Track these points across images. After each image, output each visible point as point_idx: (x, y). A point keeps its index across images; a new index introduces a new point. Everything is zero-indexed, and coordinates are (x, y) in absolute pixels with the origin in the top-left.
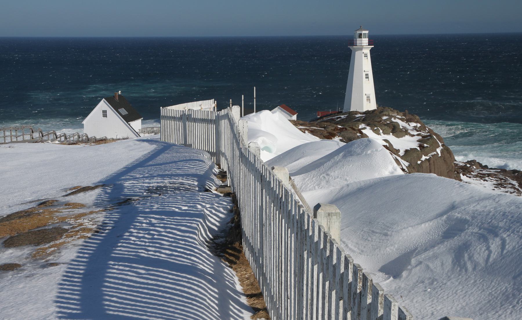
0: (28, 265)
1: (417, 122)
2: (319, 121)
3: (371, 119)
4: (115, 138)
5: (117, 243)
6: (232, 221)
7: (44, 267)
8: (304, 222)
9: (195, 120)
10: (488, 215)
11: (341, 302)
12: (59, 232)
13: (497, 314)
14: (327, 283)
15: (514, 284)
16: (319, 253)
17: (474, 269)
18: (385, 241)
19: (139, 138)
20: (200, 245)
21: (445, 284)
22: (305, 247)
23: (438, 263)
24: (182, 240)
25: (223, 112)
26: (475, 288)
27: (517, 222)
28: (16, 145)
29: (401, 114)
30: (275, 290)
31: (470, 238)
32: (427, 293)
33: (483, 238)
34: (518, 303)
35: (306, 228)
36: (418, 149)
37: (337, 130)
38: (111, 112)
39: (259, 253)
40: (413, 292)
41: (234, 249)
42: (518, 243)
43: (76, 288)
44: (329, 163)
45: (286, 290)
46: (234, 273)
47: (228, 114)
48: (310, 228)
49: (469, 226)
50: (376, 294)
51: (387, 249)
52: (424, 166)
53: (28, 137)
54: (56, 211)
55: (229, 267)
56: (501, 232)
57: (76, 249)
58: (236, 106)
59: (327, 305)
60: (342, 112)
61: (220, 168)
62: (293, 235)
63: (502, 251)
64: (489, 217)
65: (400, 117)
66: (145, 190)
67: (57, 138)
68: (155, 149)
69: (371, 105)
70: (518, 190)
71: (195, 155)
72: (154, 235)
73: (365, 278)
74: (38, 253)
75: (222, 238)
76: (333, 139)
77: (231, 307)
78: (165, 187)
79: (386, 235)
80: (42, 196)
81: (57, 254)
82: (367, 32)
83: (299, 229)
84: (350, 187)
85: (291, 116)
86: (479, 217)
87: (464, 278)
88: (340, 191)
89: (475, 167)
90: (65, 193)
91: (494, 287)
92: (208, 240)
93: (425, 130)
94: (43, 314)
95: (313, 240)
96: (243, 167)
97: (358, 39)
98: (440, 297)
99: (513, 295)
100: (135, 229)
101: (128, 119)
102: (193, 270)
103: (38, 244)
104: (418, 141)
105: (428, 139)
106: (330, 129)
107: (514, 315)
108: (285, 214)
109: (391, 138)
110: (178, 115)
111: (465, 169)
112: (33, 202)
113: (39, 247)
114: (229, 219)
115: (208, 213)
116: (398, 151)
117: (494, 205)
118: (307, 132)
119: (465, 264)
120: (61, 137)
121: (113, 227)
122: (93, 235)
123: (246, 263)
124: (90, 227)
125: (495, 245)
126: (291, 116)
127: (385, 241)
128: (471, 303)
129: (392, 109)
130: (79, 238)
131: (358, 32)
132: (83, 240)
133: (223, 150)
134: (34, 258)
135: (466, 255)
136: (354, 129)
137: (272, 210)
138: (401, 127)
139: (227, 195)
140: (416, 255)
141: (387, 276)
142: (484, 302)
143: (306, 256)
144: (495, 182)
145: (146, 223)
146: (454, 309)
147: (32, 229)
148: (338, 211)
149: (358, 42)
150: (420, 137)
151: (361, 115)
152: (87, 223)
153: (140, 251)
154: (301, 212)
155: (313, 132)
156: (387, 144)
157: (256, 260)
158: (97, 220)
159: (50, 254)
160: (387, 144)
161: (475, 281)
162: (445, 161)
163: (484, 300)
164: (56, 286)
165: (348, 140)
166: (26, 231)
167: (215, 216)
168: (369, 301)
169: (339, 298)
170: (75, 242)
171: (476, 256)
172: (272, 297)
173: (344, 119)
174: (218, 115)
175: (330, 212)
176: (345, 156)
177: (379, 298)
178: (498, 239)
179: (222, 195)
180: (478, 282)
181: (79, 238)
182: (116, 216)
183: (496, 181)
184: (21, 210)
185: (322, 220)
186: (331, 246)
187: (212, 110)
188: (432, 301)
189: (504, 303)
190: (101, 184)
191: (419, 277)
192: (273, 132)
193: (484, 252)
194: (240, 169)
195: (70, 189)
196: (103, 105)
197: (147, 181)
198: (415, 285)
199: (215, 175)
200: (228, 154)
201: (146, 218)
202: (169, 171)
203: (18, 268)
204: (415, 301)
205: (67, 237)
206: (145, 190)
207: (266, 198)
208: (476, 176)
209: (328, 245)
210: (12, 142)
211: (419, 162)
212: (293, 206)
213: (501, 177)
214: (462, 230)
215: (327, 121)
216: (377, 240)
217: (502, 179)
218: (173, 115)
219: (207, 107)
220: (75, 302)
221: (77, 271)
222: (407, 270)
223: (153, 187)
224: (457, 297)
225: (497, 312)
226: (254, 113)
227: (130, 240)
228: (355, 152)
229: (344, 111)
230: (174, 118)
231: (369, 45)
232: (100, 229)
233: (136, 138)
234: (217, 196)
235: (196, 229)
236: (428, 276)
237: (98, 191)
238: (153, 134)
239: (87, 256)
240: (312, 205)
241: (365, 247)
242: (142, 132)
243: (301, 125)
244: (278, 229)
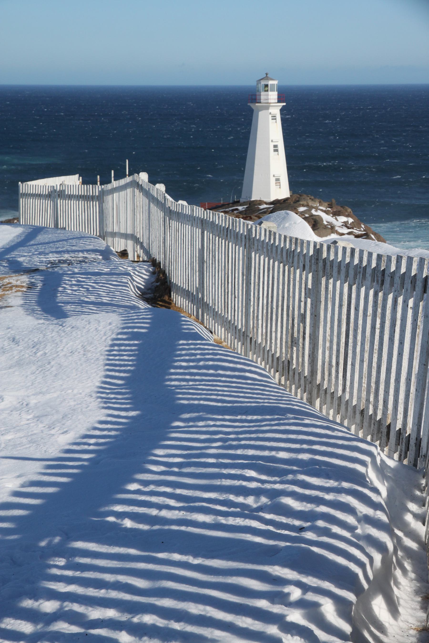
1: (348, 216)
6: (157, 280)
9: (70, 197)
22: (252, 250)
29: (326, 204)
60: (238, 202)
65: (324, 209)
69: (283, 192)
82: (275, 82)
92: (138, 295)
93: (360, 227)
114: (153, 280)
129: (312, 197)
131: (263, 83)
138: (325, 223)
145: (75, 281)
148: (275, 225)
149: (262, 97)
151: (268, 206)
167: (141, 277)
202: (62, 248)
229: (242, 200)
230: (39, 196)
231: (279, 101)
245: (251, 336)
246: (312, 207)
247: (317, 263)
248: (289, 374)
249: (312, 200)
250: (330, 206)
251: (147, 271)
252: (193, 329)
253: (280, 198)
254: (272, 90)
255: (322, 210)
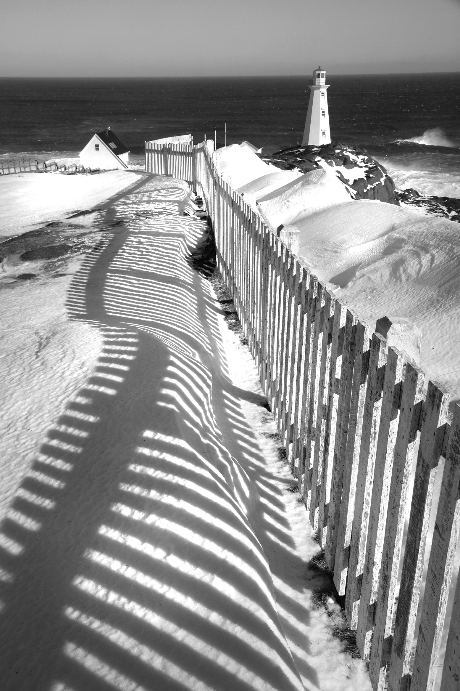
0: (42, 275)
1: (365, 155)
2: (281, 154)
3: (326, 152)
4: (107, 169)
5: (113, 258)
6: (208, 240)
7: (54, 277)
8: (269, 240)
9: (175, 153)
10: (422, 235)
11: (299, 306)
12: (65, 249)
13: (423, 316)
14: (288, 291)
15: (439, 292)
16: (281, 266)
17: (407, 280)
18: (335, 257)
19: (127, 169)
20: (181, 260)
21: (383, 292)
22: (269, 262)
23: (378, 275)
24: (166, 256)
25: (199, 146)
26: (407, 295)
27: (446, 241)
28: (24, 175)
30: (243, 297)
31: (405, 255)
32: (367, 299)
33: (416, 254)
34: (440, 307)
35: (271, 245)
36: (365, 179)
37: (297, 162)
38: (103, 146)
39: (230, 267)
40: (356, 299)
41: (209, 264)
42: (445, 258)
43: (81, 294)
44: (290, 191)
45: (253, 297)
46: (210, 283)
47: (203, 147)
48: (275, 245)
49: (405, 244)
50: (328, 300)
51: (337, 264)
52: (369, 194)
53: (34, 168)
54: (62, 231)
55: (206, 278)
56: (431, 249)
57: (80, 262)
58: (210, 140)
59: (287, 308)
61: (196, 195)
62: (260, 251)
63: (431, 265)
64: (423, 236)
65: (351, 151)
66: (134, 214)
67: (58, 169)
68: (142, 179)
69: (326, 140)
70: (446, 214)
71: (175, 184)
72: (142, 252)
73: (320, 286)
74: (49, 265)
75: (199, 254)
76: (293, 170)
77: (207, 311)
78: (150, 211)
79: (336, 252)
80: (49, 219)
81: (64, 267)
82: (324, 72)
83: (265, 247)
84: (307, 212)
85: (257, 150)
86: (414, 237)
87: (399, 288)
88: (297, 217)
89: (412, 195)
90: (67, 216)
91: (422, 294)
92: (188, 256)
93: (372, 162)
94: (57, 314)
95: (277, 255)
96: (216, 193)
97: (317, 79)
98: (378, 303)
99: (438, 300)
100: (127, 246)
101: (117, 152)
102: (175, 281)
103: (49, 258)
104: (365, 172)
105: (374, 170)
106: (291, 161)
107: (437, 316)
108: (253, 233)
109: (342, 169)
110: (160, 149)
111: (404, 197)
112: (42, 223)
113: (49, 261)
114: (205, 239)
115: (188, 234)
116: (348, 181)
117: (428, 226)
118: (270, 164)
119: (400, 276)
120: (61, 168)
121: (109, 245)
122: (92, 251)
123: (220, 276)
124: (90, 244)
125: (425, 259)
126: (257, 150)
127: (335, 257)
128: (403, 307)
130: (81, 254)
131: (317, 72)
132: (85, 255)
133: (199, 179)
134: (46, 269)
135: (401, 269)
136: (311, 162)
137: (241, 230)
138: (351, 160)
139: (203, 218)
140: (361, 269)
141: (335, 286)
142: (413, 307)
143: (270, 269)
144: (428, 208)
146: (389, 312)
147: (41, 246)
148: (298, 231)
149: (316, 82)
150: (367, 169)
152: (87, 241)
153: (132, 265)
154: (267, 232)
155: (276, 164)
156: (339, 175)
157: (228, 273)
158: (95, 239)
159: (59, 267)
160: (339, 175)
161: (408, 290)
162: (387, 189)
163: (414, 305)
164: (65, 292)
165: (306, 171)
166: (39, 247)
168: (323, 305)
169: (298, 303)
170: (78, 257)
171: (409, 270)
172: (241, 303)
173: (302, 152)
174: (194, 148)
175: (291, 232)
176: (303, 185)
177: (331, 303)
178: (428, 256)
179: (199, 218)
180: (410, 290)
181: (81, 254)
182: (111, 235)
183: (429, 206)
184: (33, 230)
185: (284, 238)
186: (291, 260)
187: (189, 144)
188: (372, 306)
189: (429, 307)
190: (97, 208)
191: (362, 287)
192: (240, 163)
193: (416, 266)
194: (214, 196)
195: (72, 213)
196: (95, 140)
197: (136, 206)
198: (358, 294)
199: (192, 200)
200: (204, 184)
201: (135, 237)
203: (35, 278)
204: (357, 306)
205: (72, 252)
206: (134, 214)
207: (237, 221)
208: (413, 203)
209: (290, 259)
210: (21, 172)
211: (365, 191)
212: (260, 227)
213: (433, 203)
214: (399, 248)
215: (287, 154)
216: (329, 257)
217: (434, 205)
218: (156, 148)
219: (185, 141)
220: (81, 305)
221: (82, 281)
222: (352, 281)
223: (141, 211)
224: (392, 303)
225: (423, 314)
226: (225, 147)
227: (123, 255)
228: (312, 181)
229: (302, 145)
230: (156, 151)
232: (98, 246)
233: (125, 169)
234: (195, 219)
235: (178, 247)
236: (369, 286)
237: (95, 214)
238: (139, 166)
239: (89, 268)
240: (274, 226)
241: (318, 262)
242: (129, 164)
243: (266, 157)
244: (246, 246)
245: (266, 362)
246: (344, 150)
247: (352, 350)
248: (304, 465)
249: (344, 145)
250: (354, 149)
251: (202, 230)
252: (171, 400)
253: (325, 144)
254: (323, 77)
255: (349, 152)
